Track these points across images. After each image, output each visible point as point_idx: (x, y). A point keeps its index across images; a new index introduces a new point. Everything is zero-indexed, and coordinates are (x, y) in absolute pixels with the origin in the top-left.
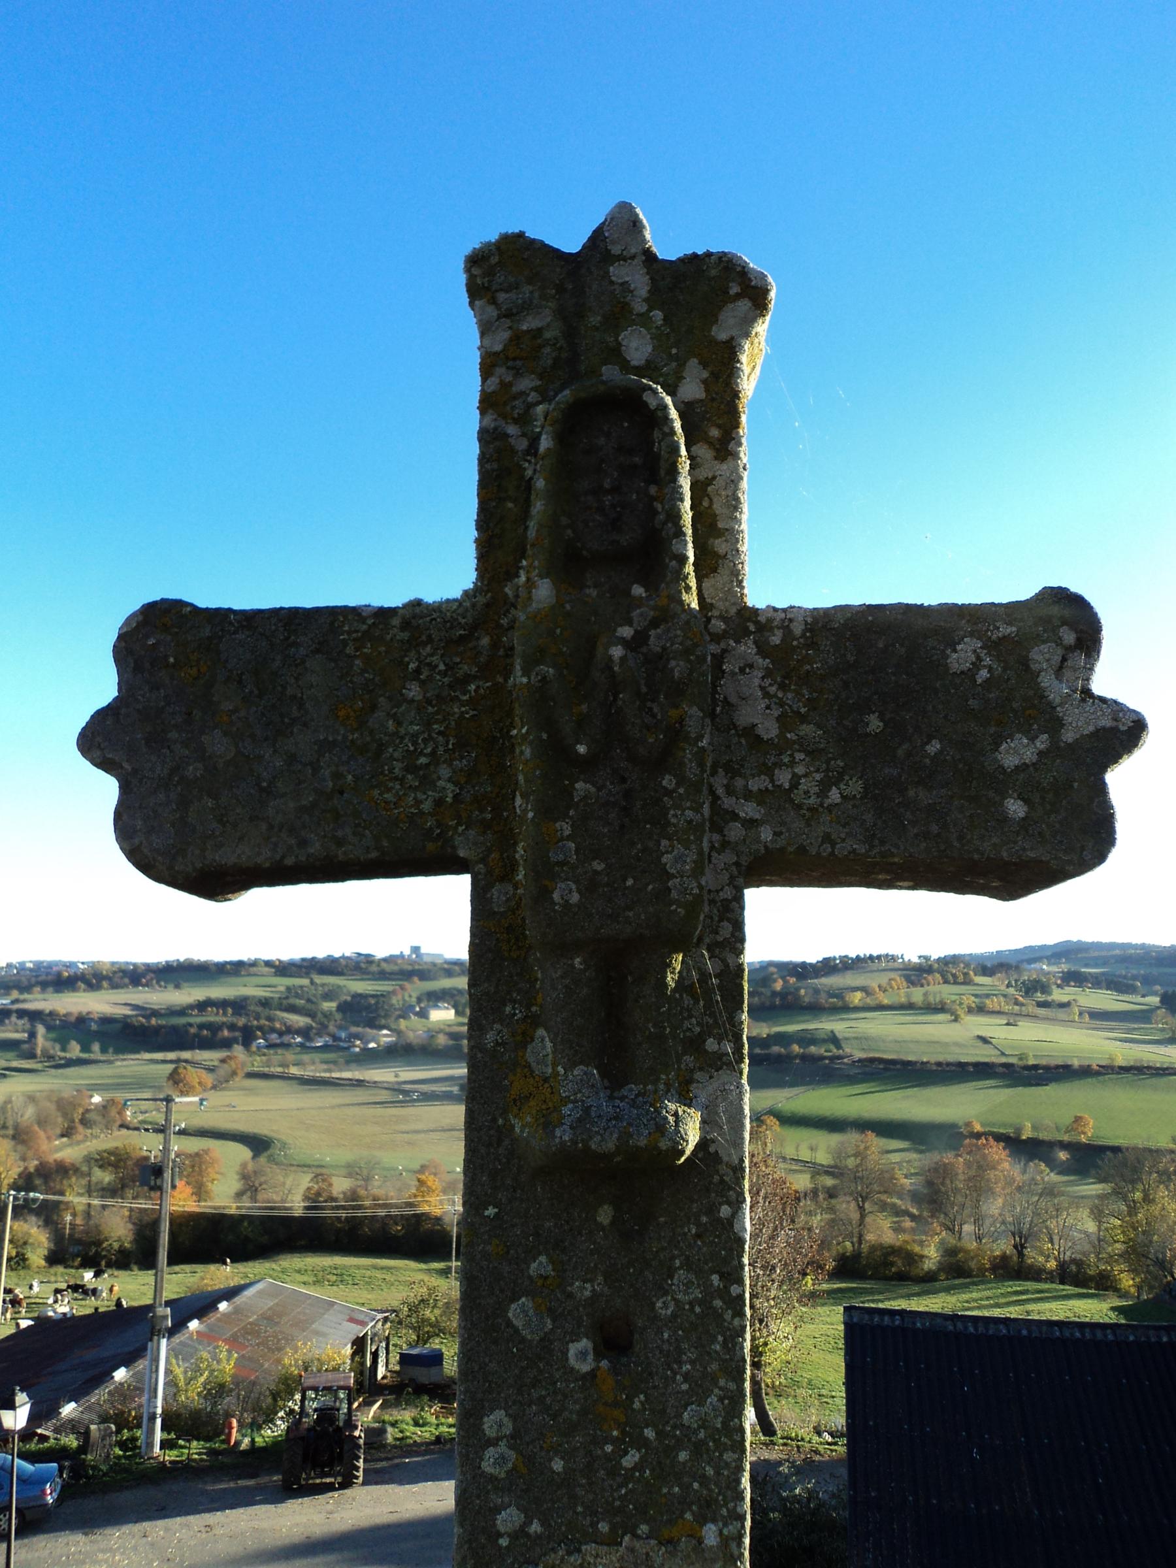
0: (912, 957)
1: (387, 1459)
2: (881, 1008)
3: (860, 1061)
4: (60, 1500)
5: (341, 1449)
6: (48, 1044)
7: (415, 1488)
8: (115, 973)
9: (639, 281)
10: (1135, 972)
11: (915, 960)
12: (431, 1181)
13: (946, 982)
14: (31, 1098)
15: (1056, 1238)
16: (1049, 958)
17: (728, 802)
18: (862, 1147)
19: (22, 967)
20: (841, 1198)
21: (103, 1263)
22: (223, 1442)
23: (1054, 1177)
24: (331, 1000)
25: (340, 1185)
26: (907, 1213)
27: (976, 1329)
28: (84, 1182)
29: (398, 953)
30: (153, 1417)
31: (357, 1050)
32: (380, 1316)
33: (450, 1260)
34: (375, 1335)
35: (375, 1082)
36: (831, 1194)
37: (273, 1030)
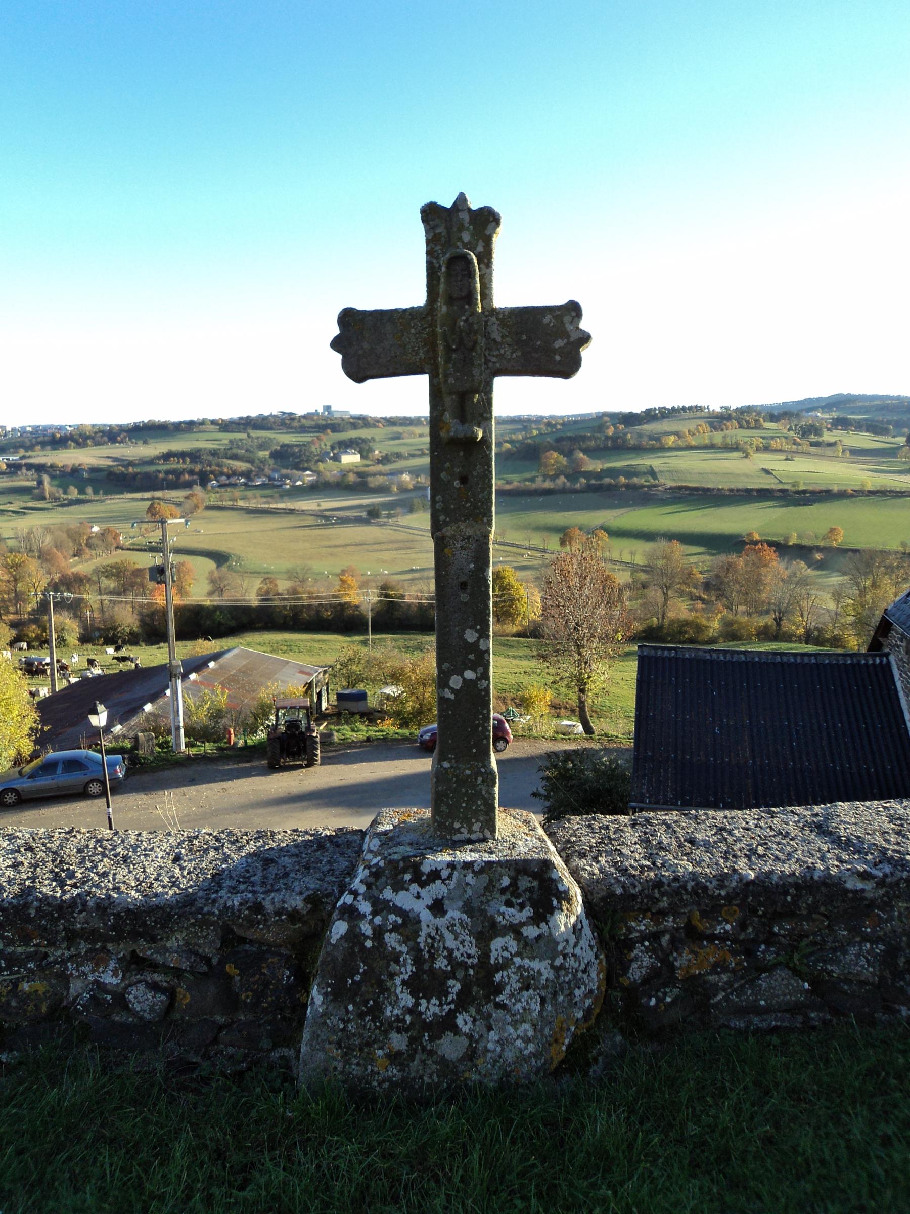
0: (716, 407)
1: (336, 751)
2: (690, 448)
3: (671, 488)
4: (127, 776)
5: (305, 744)
6: (54, 489)
7: (355, 766)
8: (96, 433)
9: (465, 217)
10: (889, 418)
11: (718, 410)
12: (349, 580)
13: (741, 427)
14: (48, 529)
15: (805, 614)
16: (823, 408)
17: (489, 358)
18: (669, 551)
19: (23, 431)
20: (652, 588)
21: (120, 642)
22: (225, 743)
23: (810, 572)
24: (265, 450)
25: (283, 586)
26: (700, 598)
27: (725, 658)
28: (96, 587)
29: (314, 411)
30: (178, 728)
31: (288, 486)
32: (321, 670)
33: (368, 634)
34: (318, 682)
35: (303, 511)
36: (644, 586)
37: (222, 474)
